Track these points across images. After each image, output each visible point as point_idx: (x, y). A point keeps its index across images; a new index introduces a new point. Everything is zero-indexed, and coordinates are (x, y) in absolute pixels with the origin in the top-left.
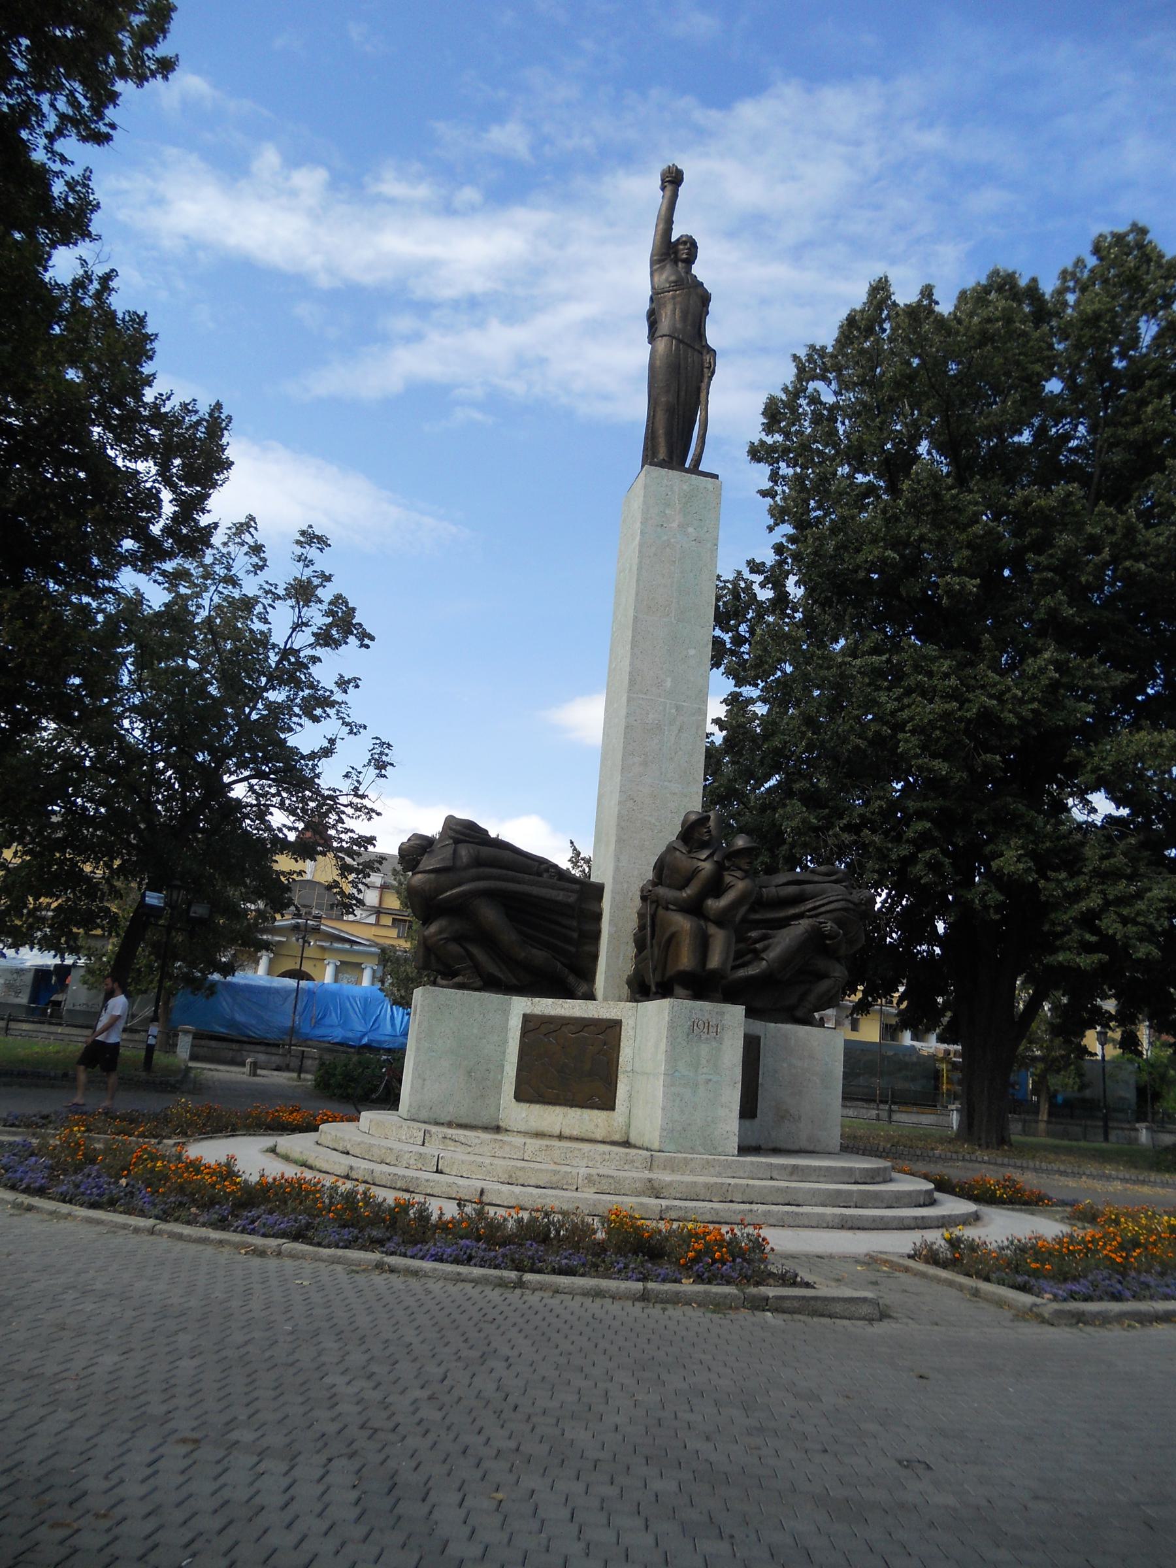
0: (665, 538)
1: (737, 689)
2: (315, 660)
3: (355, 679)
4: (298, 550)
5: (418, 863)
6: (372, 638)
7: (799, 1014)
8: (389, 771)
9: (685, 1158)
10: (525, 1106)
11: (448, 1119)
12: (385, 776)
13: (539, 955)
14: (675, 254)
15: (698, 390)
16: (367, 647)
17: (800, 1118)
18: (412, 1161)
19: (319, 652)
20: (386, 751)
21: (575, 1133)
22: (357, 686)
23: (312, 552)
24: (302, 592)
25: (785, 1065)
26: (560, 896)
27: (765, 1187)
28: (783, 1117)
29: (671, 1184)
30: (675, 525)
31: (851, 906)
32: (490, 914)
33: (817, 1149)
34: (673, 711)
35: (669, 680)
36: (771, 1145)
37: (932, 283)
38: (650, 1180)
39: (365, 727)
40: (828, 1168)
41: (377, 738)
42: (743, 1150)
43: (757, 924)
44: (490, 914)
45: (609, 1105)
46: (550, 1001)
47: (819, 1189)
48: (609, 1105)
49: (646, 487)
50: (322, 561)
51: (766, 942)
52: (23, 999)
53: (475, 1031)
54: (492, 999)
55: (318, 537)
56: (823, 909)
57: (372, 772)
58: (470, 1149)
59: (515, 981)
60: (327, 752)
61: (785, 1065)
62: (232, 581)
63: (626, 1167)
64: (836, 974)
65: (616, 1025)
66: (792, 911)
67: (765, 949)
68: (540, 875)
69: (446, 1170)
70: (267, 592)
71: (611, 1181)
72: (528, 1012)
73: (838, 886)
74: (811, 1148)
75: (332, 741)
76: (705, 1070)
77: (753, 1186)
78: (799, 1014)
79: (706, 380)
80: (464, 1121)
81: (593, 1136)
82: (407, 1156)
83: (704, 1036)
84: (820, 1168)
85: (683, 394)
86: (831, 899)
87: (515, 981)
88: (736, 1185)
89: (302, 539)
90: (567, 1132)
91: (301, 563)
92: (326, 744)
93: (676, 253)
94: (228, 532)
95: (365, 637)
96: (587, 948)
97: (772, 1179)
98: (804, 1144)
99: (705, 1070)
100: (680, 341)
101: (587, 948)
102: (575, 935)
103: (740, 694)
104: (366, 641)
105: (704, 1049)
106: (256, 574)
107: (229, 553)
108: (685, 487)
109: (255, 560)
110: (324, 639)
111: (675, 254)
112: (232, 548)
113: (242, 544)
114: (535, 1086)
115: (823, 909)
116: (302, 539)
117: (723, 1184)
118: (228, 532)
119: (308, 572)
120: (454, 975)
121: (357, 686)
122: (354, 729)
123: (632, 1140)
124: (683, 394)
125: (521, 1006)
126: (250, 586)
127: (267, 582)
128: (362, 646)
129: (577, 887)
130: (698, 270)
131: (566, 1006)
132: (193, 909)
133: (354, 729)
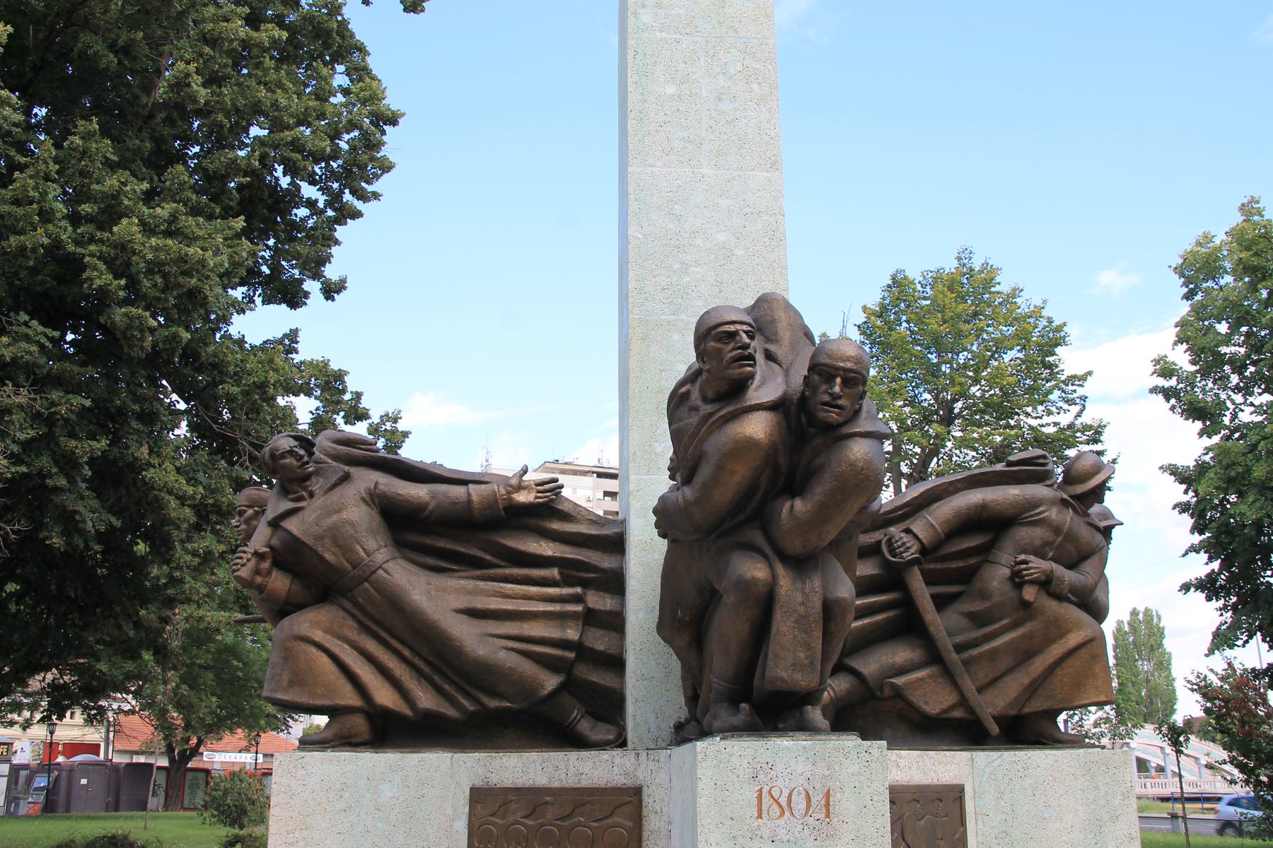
59: (426, 699)
65: (955, 795)
87: (426, 699)
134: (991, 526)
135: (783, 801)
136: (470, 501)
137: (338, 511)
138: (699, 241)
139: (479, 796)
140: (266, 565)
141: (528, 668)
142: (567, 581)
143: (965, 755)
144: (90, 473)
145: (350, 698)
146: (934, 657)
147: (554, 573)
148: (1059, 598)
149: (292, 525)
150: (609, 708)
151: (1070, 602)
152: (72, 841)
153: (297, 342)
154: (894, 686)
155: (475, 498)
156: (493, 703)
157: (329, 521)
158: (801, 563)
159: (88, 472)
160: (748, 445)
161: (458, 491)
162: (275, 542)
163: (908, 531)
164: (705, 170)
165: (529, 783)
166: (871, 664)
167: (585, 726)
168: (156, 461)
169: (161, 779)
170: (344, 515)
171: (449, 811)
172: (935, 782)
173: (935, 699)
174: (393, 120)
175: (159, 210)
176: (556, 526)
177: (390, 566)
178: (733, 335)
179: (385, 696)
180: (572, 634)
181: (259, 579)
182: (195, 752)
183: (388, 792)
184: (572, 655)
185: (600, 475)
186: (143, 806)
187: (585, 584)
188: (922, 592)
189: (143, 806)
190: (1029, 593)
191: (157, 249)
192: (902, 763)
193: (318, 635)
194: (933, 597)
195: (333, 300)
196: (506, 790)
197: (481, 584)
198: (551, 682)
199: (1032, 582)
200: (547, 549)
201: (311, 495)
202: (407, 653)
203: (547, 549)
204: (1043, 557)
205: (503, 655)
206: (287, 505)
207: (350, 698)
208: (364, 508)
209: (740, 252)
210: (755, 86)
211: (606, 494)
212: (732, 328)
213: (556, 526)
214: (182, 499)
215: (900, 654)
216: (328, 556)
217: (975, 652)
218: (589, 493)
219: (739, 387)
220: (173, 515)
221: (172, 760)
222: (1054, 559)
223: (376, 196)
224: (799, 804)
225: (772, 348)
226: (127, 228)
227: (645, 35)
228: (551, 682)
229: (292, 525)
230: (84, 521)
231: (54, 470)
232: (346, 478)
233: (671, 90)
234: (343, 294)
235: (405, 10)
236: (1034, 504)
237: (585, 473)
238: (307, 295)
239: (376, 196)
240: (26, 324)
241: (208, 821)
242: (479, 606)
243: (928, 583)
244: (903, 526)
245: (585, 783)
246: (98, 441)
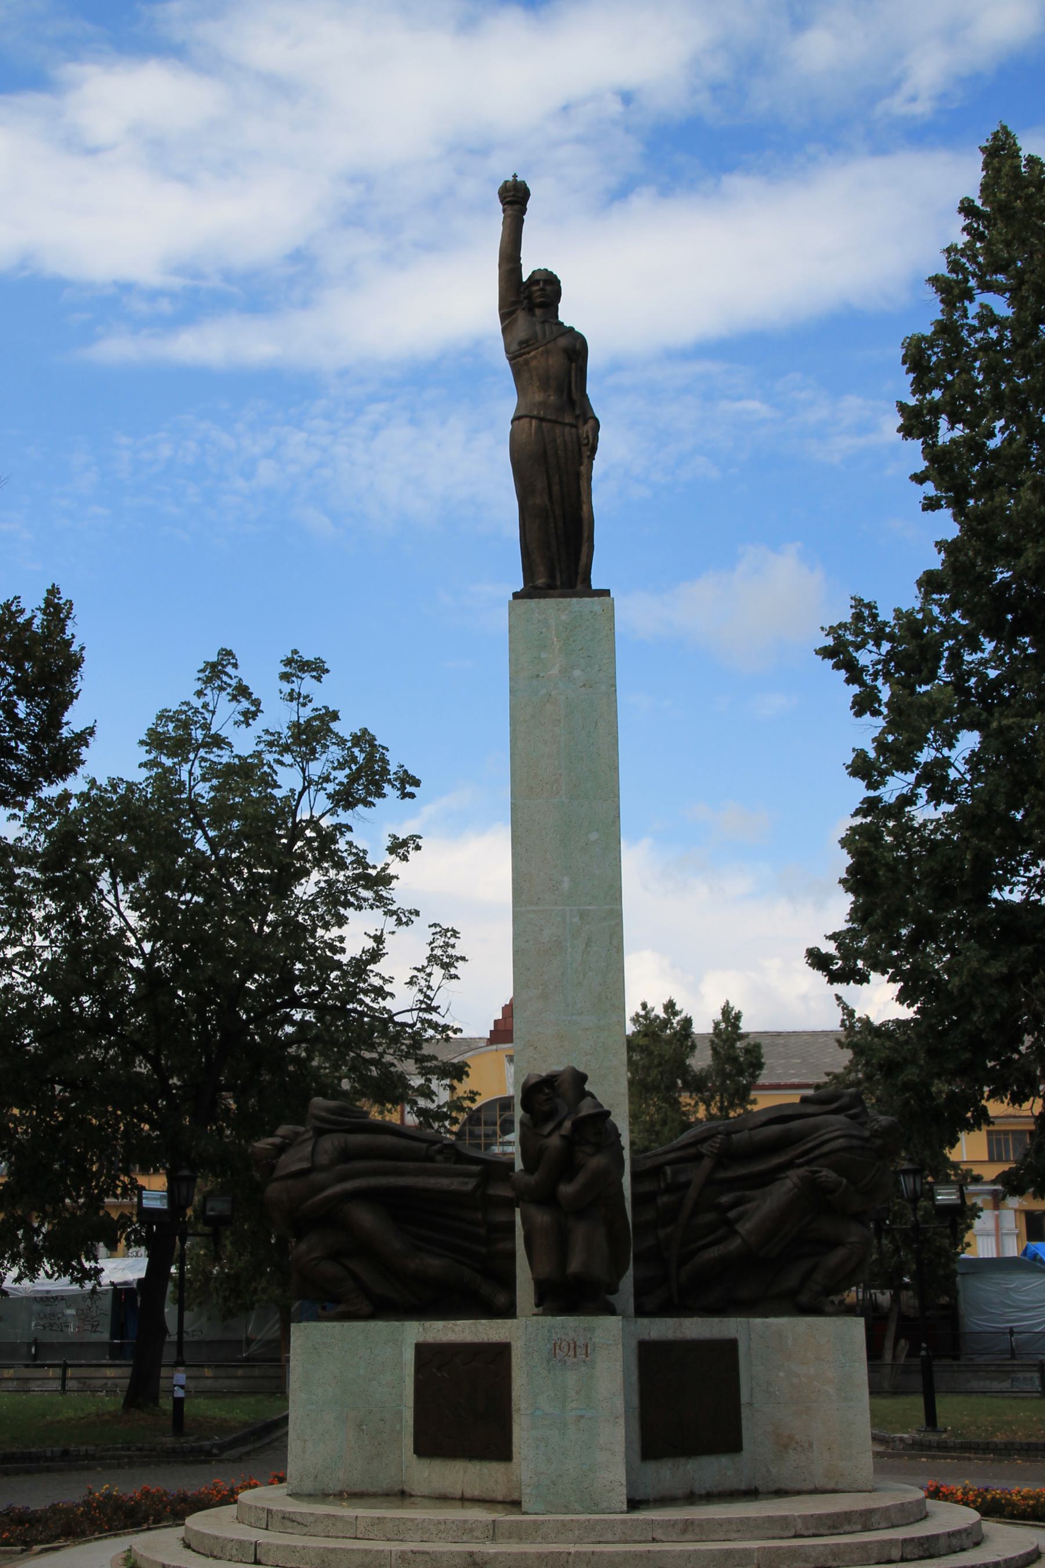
0: (544, 691)
1: (872, 793)
2: (342, 828)
3: (414, 838)
4: (287, 687)
5: (273, 1168)
6: (417, 783)
7: (804, 1299)
8: (460, 968)
9: (535, 1522)
10: (425, 1463)
11: (338, 1488)
12: (456, 977)
13: (434, 1264)
14: (529, 299)
15: (578, 475)
16: (412, 796)
17: (811, 1445)
18: (234, 1552)
19: (344, 817)
20: (452, 941)
22: (418, 848)
23: (307, 684)
24: (310, 735)
25: (782, 1374)
26: (454, 1184)
27: (617, 1554)
28: (786, 1447)
29: (497, 1554)
30: (555, 671)
31: (855, 1142)
32: (365, 1218)
33: (840, 1487)
34: (576, 920)
35: (566, 879)
36: (774, 1487)
38: (471, 1554)
39: (417, 913)
40: (743, 1521)
41: (435, 925)
42: (634, 1504)
43: (731, 1184)
44: (365, 1218)
47: (779, 1548)
50: (322, 694)
51: (741, 1209)
52: (105, 1336)
53: (362, 1372)
54: (379, 1327)
55: (308, 663)
56: (817, 1153)
57: (438, 972)
58: (306, 1530)
60: (375, 956)
61: (782, 1374)
62: (218, 741)
63: (465, 1538)
64: (853, 1239)
66: (776, 1161)
67: (740, 1218)
68: (431, 1159)
69: (263, 1559)
70: (270, 744)
71: (427, 1558)
72: (421, 1340)
73: (841, 1118)
74: (831, 1486)
75: (379, 939)
76: (574, 1405)
77: (601, 1553)
78: (804, 1299)
79: (586, 461)
80: (357, 1489)
83: (570, 1360)
84: (729, 1521)
85: (556, 488)
86: (826, 1137)
88: (578, 1553)
89: (288, 669)
90: (468, 1494)
91: (295, 703)
92: (371, 944)
93: (529, 297)
94: (201, 675)
95: (407, 782)
96: (501, 1246)
97: (654, 1540)
98: (821, 1482)
99: (574, 1405)
100: (541, 420)
101: (501, 1246)
102: (482, 1231)
103: (879, 799)
104: (409, 789)
105: (571, 1378)
106: (248, 725)
107: (205, 706)
108: (564, 617)
109: (245, 704)
110: (344, 799)
111: (529, 299)
112: (210, 696)
113: (221, 689)
114: (435, 1439)
115: (817, 1153)
116: (288, 669)
117: (560, 1553)
118: (201, 675)
119: (306, 713)
120: (337, 1300)
121: (418, 848)
122: (404, 918)
124: (556, 488)
125: (416, 1331)
126: (244, 742)
127: (267, 732)
128: (405, 795)
129: (475, 1168)
130: (568, 314)
131: (457, 1329)
132: (209, 1206)
133: (404, 918)
172: (486, 1340)
192: (457, 1329)
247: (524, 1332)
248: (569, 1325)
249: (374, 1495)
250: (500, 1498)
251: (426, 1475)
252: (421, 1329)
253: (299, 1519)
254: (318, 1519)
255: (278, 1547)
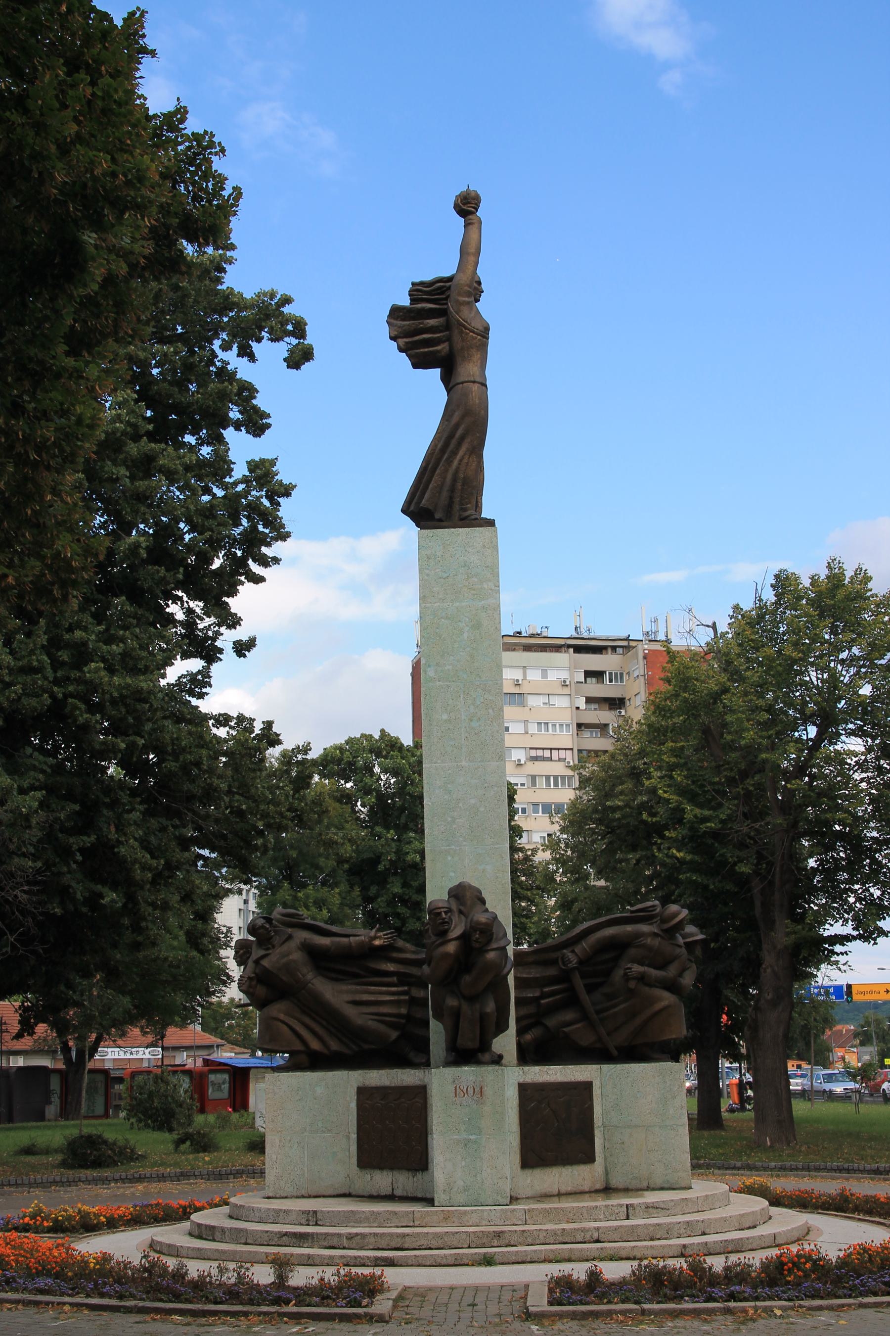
10: (528, 1172)
18: (682, 1231)
21: (569, 1189)
37: (735, 603)
45: (589, 1158)
46: (537, 1068)
48: (589, 1158)
49: (217, 487)
59: (335, 1046)
65: (587, 1087)
72: (521, 1081)
81: (581, 1188)
82: (676, 1227)
87: (335, 1046)
90: (563, 1190)
123: (615, 1182)
131: (550, 1072)
134: (617, 948)
135: (465, 1090)
136: (350, 943)
137: (288, 955)
138: (461, 805)
139: (362, 1092)
140: (254, 983)
141: (382, 1028)
142: (401, 983)
143: (598, 1066)
144: (81, 858)
145: (299, 1046)
146: (585, 1017)
147: (395, 979)
148: (650, 985)
149: (265, 963)
150: (423, 1046)
151: (657, 987)
152: (33, 1145)
153: (210, 677)
154: (564, 1032)
155: (353, 945)
156: (366, 1047)
157: (285, 960)
158: (471, 999)
159: (79, 858)
160: (446, 955)
161: (345, 940)
162: (257, 971)
163: (573, 951)
164: (464, 763)
165: (382, 1084)
166: (552, 1022)
167: (412, 1055)
168: (123, 839)
169: (55, 1084)
170: (291, 957)
171: (348, 1099)
172: (573, 1080)
173: (586, 1039)
174: (287, 491)
175: (114, 647)
176: (395, 955)
177: (314, 981)
178: (440, 913)
179: (315, 1045)
180: (404, 1011)
181: (251, 990)
182: (94, 1049)
183: (319, 1090)
184: (403, 1021)
185: (578, 649)
186: (41, 1117)
187: (409, 984)
188: (579, 982)
189: (41, 1117)
190: (632, 984)
191: (120, 688)
192: (550, 1072)
193: (282, 1016)
194: (585, 986)
195: (245, 656)
196: (372, 1088)
197: (358, 987)
198: (394, 1035)
199: (634, 978)
200: (391, 967)
201: (274, 947)
202: (324, 1023)
203: (391, 967)
204: (642, 965)
205: (370, 1023)
206: (262, 952)
207: (299, 1046)
208: (300, 952)
209: (482, 809)
210: (490, 711)
211: (588, 674)
212: (439, 911)
213: (395, 955)
214: (145, 867)
215: (568, 1015)
216: (284, 978)
217: (605, 1014)
218: (564, 675)
219: (445, 933)
220: (138, 878)
221: (68, 1060)
222: (649, 966)
223: (276, 560)
224: (471, 1092)
225: (462, 908)
226: (94, 669)
227: (431, 684)
228: (394, 1035)
229: (265, 963)
230: (75, 893)
231: (57, 860)
232: (290, 937)
233: (445, 717)
234: (254, 651)
235: (288, 367)
236: (638, 935)
237: (557, 648)
238: (221, 651)
239: (276, 560)
240: (31, 756)
241: (135, 1125)
242: (358, 999)
243: (582, 978)
244: (571, 949)
245: (405, 1084)
246: (89, 836)
247: (443, 1082)
248: (467, 1073)
249: (582, 1193)
250: (587, 1190)
251: (529, 1181)
252: (521, 1073)
253: (662, 1206)
254: (676, 1203)
255: (716, 1220)
